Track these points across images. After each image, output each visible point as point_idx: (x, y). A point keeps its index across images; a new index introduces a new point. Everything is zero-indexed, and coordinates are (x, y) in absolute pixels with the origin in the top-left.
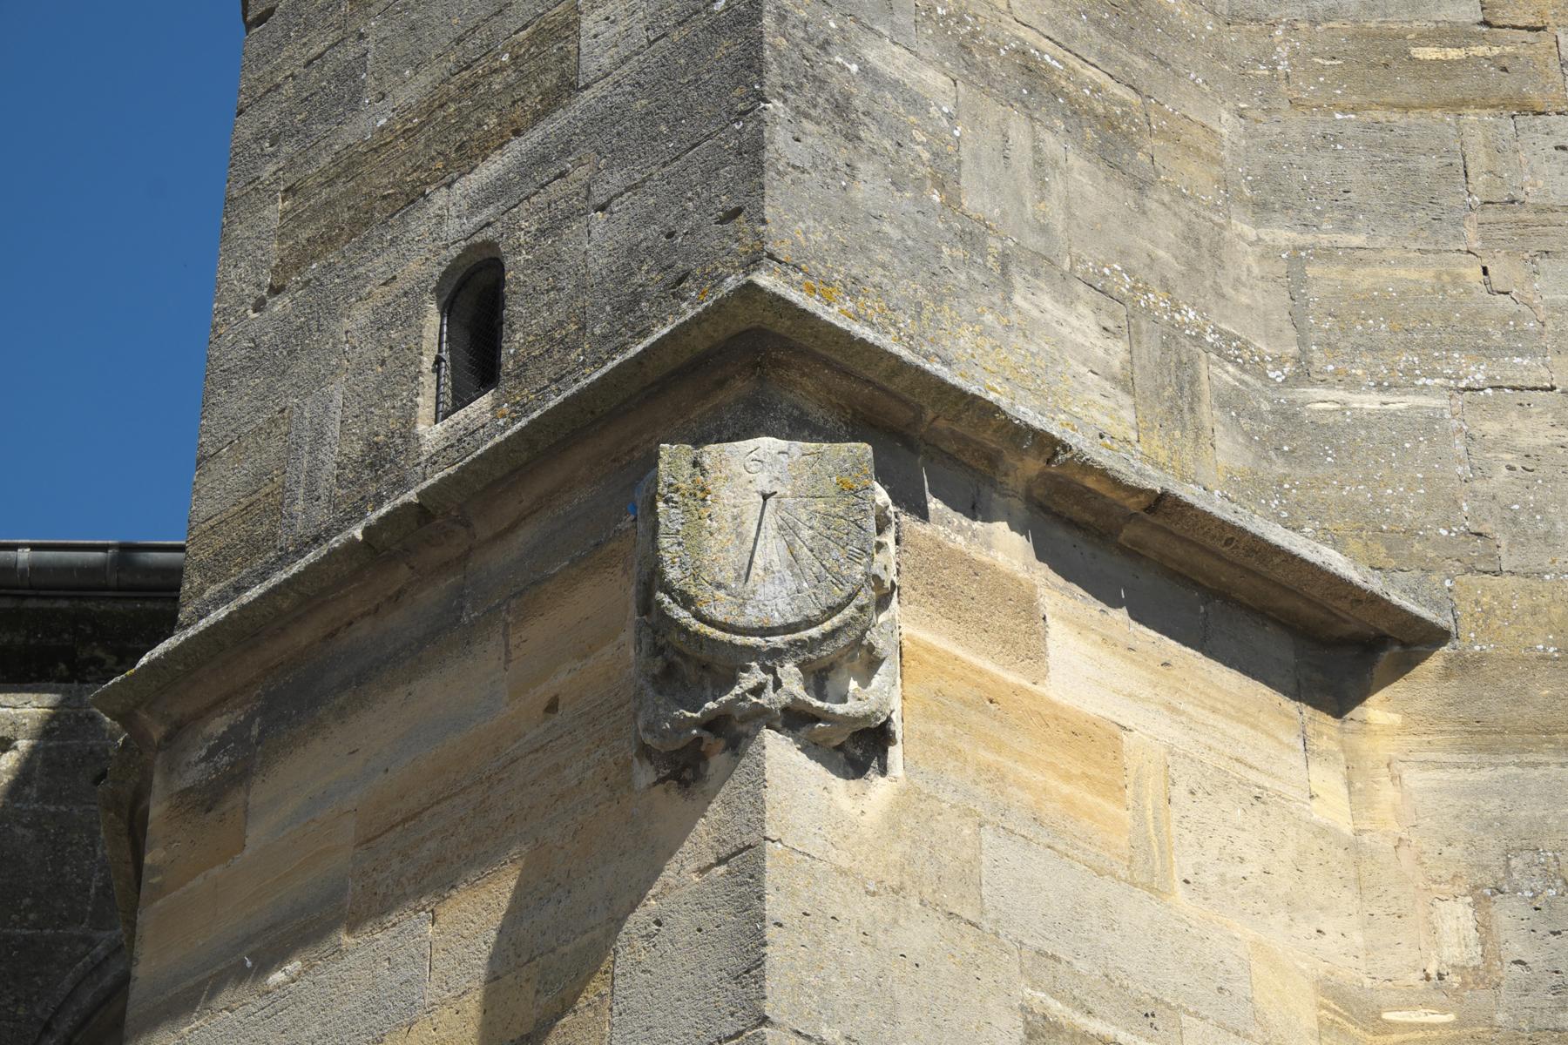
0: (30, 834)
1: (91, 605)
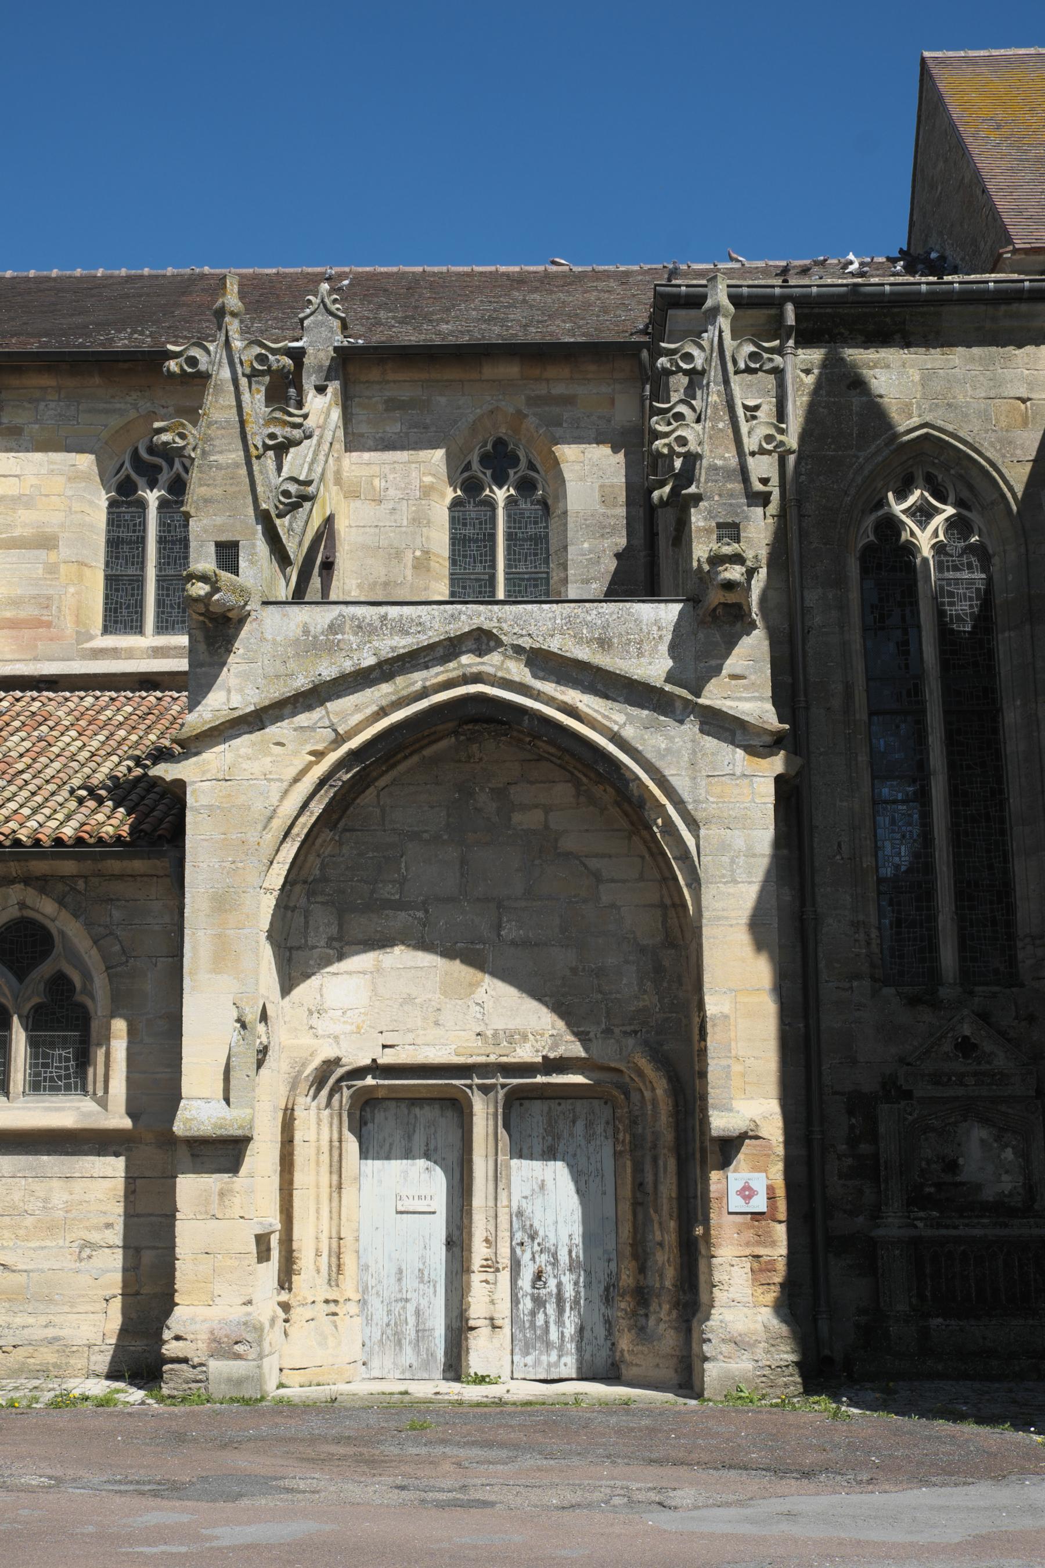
0: (826, 411)
1: (841, 310)
